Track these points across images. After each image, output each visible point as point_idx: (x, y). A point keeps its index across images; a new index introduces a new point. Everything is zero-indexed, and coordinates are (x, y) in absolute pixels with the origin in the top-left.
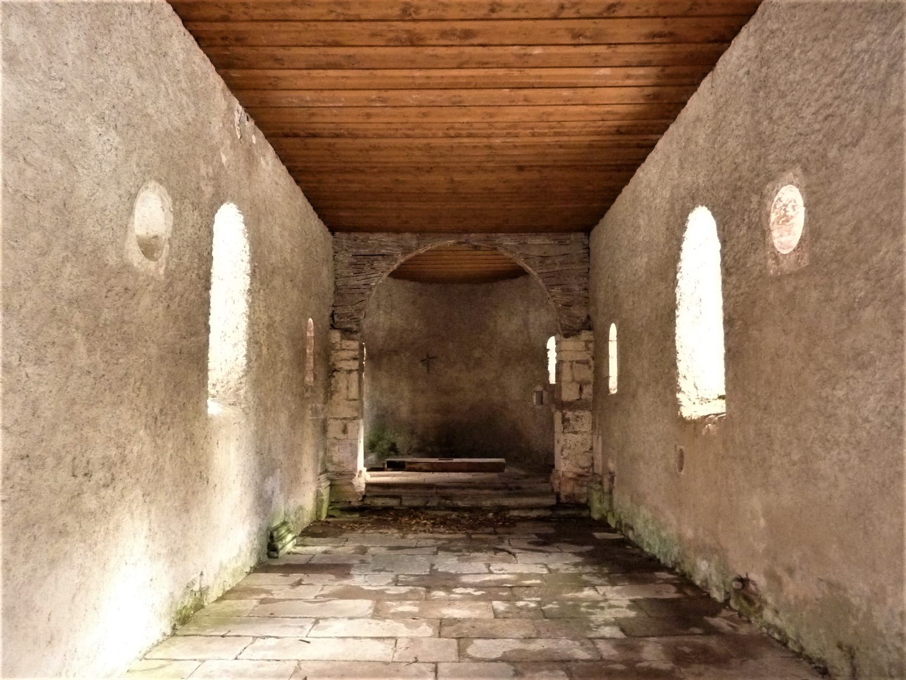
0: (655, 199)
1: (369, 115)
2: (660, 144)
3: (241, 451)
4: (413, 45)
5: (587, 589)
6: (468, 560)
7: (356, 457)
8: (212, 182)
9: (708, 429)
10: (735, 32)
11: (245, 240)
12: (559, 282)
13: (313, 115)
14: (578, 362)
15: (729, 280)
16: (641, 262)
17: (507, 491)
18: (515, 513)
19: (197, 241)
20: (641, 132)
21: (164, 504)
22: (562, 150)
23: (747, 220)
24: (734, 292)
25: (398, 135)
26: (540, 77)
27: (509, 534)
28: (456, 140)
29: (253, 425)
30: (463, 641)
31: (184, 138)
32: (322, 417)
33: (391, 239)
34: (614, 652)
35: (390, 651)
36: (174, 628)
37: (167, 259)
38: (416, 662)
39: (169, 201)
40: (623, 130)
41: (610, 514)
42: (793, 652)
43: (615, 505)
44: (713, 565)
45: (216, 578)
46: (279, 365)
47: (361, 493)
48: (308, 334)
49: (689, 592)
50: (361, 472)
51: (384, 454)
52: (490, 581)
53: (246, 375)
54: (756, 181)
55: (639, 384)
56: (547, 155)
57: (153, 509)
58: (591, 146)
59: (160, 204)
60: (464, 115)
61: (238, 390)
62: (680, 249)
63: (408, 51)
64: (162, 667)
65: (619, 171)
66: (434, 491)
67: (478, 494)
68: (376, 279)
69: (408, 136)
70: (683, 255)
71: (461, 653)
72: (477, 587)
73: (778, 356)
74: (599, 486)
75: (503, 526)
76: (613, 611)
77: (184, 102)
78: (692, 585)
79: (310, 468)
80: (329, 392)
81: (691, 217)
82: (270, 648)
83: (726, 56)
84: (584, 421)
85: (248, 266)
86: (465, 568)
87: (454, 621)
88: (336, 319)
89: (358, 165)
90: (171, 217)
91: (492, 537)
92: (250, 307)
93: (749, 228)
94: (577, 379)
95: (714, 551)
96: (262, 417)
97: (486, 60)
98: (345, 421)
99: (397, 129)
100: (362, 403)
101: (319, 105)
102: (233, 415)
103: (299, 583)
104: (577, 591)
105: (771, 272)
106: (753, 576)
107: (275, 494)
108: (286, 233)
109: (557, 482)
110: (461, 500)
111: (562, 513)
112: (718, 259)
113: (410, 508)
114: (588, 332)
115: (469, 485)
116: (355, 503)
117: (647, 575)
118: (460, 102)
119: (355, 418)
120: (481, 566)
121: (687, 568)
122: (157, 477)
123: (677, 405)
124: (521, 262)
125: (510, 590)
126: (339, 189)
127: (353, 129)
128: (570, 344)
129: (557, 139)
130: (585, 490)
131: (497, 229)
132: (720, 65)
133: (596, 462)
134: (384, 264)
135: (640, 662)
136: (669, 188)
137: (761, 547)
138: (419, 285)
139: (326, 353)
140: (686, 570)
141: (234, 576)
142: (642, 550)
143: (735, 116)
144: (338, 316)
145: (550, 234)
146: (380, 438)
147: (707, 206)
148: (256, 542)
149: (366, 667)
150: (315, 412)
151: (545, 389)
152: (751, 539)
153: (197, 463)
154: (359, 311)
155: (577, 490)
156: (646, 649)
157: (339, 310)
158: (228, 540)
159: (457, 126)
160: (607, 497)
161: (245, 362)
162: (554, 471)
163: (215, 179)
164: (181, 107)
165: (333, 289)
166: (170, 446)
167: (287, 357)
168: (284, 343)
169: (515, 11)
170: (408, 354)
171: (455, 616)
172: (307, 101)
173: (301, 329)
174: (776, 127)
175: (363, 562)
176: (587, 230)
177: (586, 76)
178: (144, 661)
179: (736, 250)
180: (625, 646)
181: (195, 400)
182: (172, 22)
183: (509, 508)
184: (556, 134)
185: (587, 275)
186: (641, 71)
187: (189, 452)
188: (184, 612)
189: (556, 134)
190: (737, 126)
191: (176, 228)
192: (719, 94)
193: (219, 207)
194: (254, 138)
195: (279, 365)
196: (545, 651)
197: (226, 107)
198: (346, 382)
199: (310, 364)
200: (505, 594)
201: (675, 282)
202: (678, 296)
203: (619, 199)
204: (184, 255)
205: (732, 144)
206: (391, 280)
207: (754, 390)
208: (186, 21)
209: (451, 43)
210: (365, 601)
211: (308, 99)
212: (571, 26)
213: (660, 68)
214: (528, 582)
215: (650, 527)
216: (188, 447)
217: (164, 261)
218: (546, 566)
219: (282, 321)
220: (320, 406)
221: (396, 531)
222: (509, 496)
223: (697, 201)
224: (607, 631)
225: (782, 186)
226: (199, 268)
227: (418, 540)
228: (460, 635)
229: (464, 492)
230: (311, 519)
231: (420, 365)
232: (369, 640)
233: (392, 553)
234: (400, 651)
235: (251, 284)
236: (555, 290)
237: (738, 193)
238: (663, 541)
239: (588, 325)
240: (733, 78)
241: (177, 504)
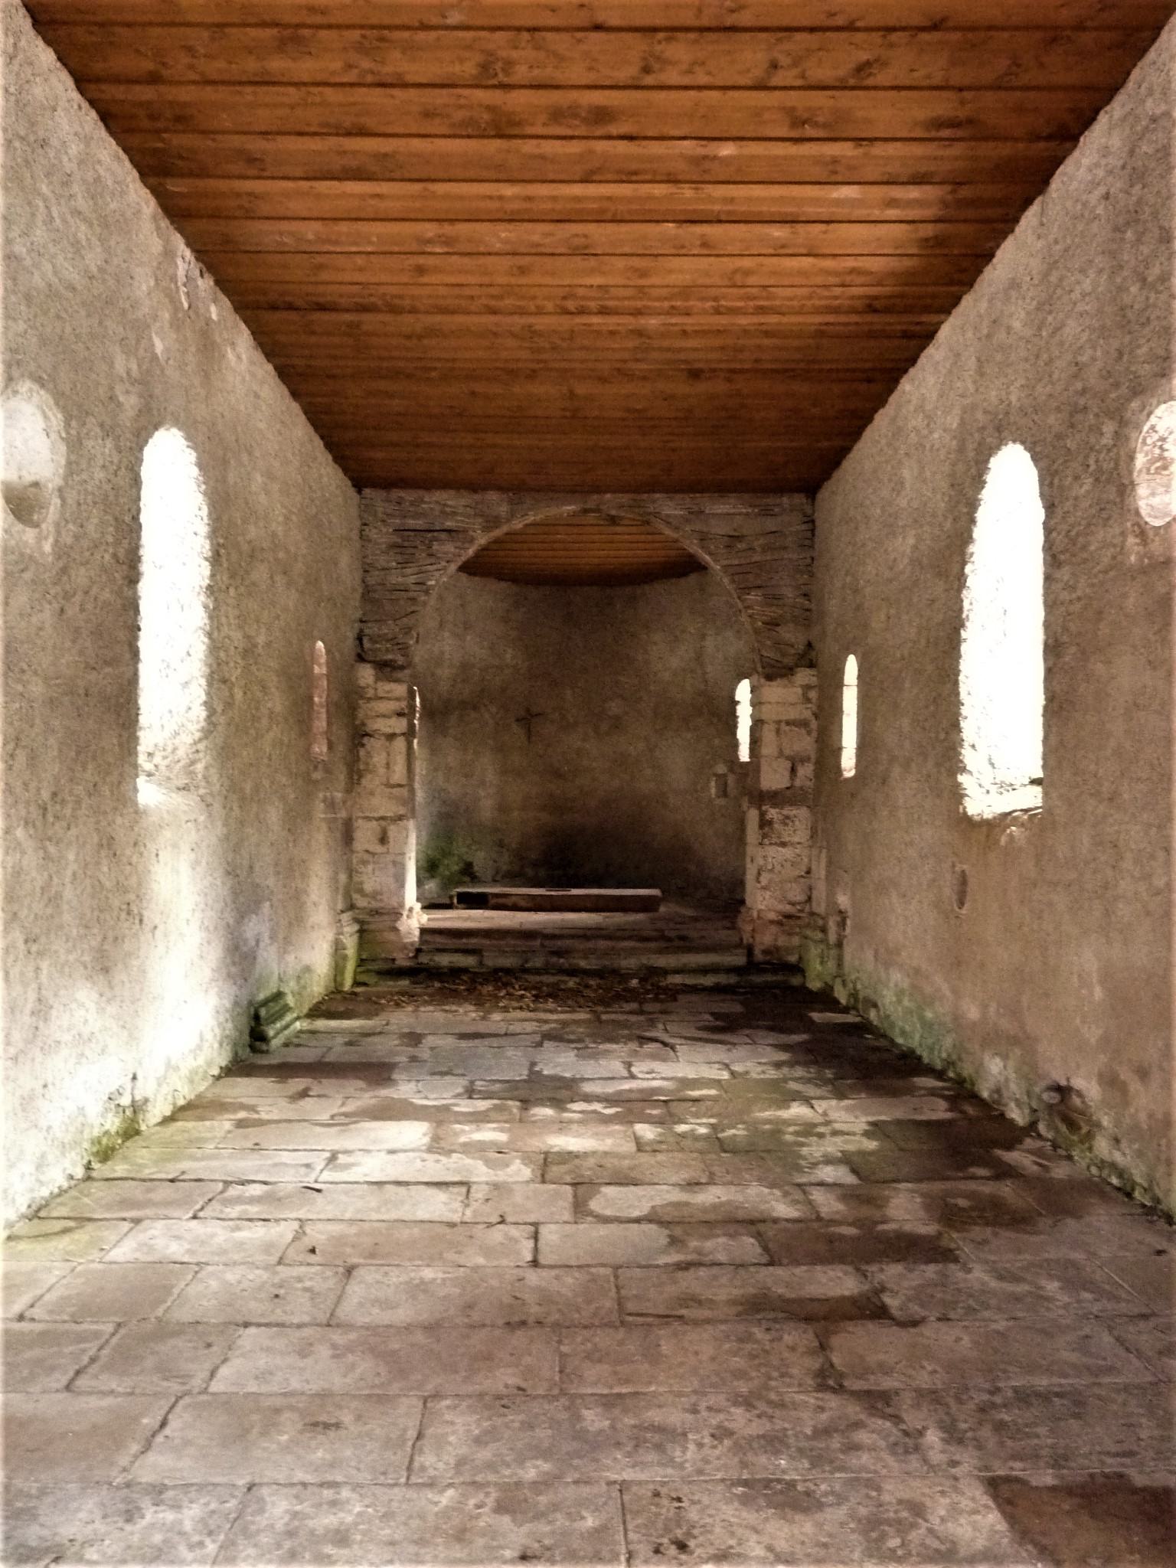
0: (931, 433)
1: (421, 270)
2: (945, 332)
3: (198, 869)
4: (501, 136)
5: (795, 1104)
6: (595, 1056)
7: (401, 884)
8: (137, 388)
9: (1011, 835)
10: (1087, 120)
11: (200, 498)
12: (759, 582)
13: (321, 267)
14: (788, 723)
15: (1057, 575)
16: (904, 545)
17: (663, 944)
18: (677, 979)
19: (111, 494)
20: (908, 310)
21: (63, 957)
22: (766, 342)
23: (1093, 467)
24: (1065, 596)
25: (473, 308)
26: (732, 200)
27: (664, 1012)
28: (579, 320)
29: (219, 824)
30: (582, 1189)
31: (84, 304)
32: (343, 814)
33: (463, 502)
34: (840, 1207)
35: (457, 1205)
36: (88, 1167)
37: (57, 525)
38: (502, 1222)
39: (57, 419)
40: (877, 304)
41: (838, 982)
42: (1144, 1206)
43: (846, 969)
44: (1011, 1063)
45: (159, 1085)
46: (265, 721)
47: (412, 944)
48: (317, 670)
49: (970, 1110)
50: (411, 910)
51: (451, 878)
52: (630, 1091)
53: (206, 738)
54: (1113, 395)
55: (893, 759)
56: (741, 350)
57: (45, 965)
58: (820, 334)
59: (41, 424)
60: (592, 271)
61: (193, 763)
62: (973, 521)
63: (492, 146)
64: (65, 1231)
65: (869, 381)
66: (538, 942)
67: (613, 948)
68: (437, 574)
69: (494, 312)
70: (977, 532)
71: (580, 1208)
72: (608, 1100)
73: (1136, 705)
74: (820, 935)
75: (656, 999)
76: (838, 1139)
77: (81, 236)
78: (974, 1097)
79: (323, 901)
80: (355, 773)
81: (994, 463)
82: (252, 1200)
83: (1067, 168)
84: (798, 824)
85: (207, 545)
86: (588, 1068)
87: (567, 1157)
88: (367, 644)
89: (401, 364)
90: (63, 448)
91: (633, 1018)
92: (211, 618)
93: (1097, 480)
94: (787, 752)
95: (1015, 1041)
96: (237, 811)
97: (634, 166)
98: (383, 823)
99: (472, 297)
100: (412, 791)
101: (332, 249)
102: (186, 808)
103: (304, 1094)
104: (780, 1108)
105: (1133, 558)
106: (1078, 1083)
107: (262, 945)
108: (276, 487)
109: (748, 928)
110: (586, 958)
111: (758, 979)
112: (1039, 538)
113: (496, 970)
114: (808, 671)
115: (586, 934)
116: (402, 961)
117: (899, 1083)
118: (586, 247)
119: (400, 818)
120: (616, 1066)
121: (967, 1070)
122: (49, 911)
123: (957, 795)
124: (694, 548)
125: (664, 1107)
126: (372, 407)
127: (394, 296)
128: (775, 691)
129: (763, 319)
130: (796, 941)
131: (652, 487)
132: (1056, 183)
133: (815, 894)
134: (450, 548)
135: (883, 1222)
136: (957, 411)
137: (1093, 1034)
138: (515, 588)
139: (348, 705)
140: (965, 1074)
141: (191, 1081)
142: (892, 1041)
143: (1079, 276)
144: (372, 640)
145: (746, 496)
146: (446, 853)
147: (1023, 443)
148: (230, 1025)
149: (416, 1231)
150: (331, 805)
151: (731, 770)
152: (1078, 1021)
153: (121, 888)
154: (407, 630)
155: (782, 941)
156: (894, 1202)
157: (372, 629)
158: (176, 1015)
159: (581, 292)
160: (833, 952)
161: (204, 714)
162: (743, 910)
163: (144, 382)
164: (76, 244)
165: (360, 590)
166: (71, 857)
167: (278, 708)
168: (272, 681)
169: (690, 72)
170: (494, 710)
171: (571, 1148)
172: (309, 241)
173: (305, 660)
174: (1153, 296)
175: (414, 1059)
176: (811, 488)
177: (816, 201)
178: (36, 1221)
179: (1071, 520)
180: (858, 1196)
181: (114, 778)
182: (54, 80)
183: (665, 972)
184: (761, 310)
185: (809, 568)
186: (914, 193)
187: (105, 869)
188: (104, 1141)
189: (761, 310)
190: (1084, 295)
191: (71, 468)
192: (1051, 237)
193: (150, 435)
194: (213, 309)
195: (265, 721)
196: (722, 1204)
197: (160, 248)
198: (384, 754)
199: (320, 723)
200: (655, 1112)
201: (961, 580)
202: (966, 605)
203: (869, 433)
204: (88, 519)
205: (1072, 328)
206: (464, 577)
207: (1092, 767)
208: (82, 81)
209: (570, 132)
210: (416, 1124)
211: (311, 236)
212: (789, 104)
213: (948, 188)
214: (696, 1093)
215: (906, 1002)
216: (105, 862)
217: (52, 529)
218: (727, 1066)
219: (268, 644)
220: (339, 795)
221: (472, 1008)
222: (660, 952)
223: (1005, 434)
224: (828, 1173)
225: (1159, 404)
226: (117, 543)
227: (509, 1022)
228: (580, 1183)
229: (590, 945)
230: (326, 987)
231: (515, 728)
232: (423, 1187)
233: (464, 1044)
234: (475, 1205)
235: (213, 576)
236: (753, 597)
237: (1079, 417)
238: (927, 1025)
239: (808, 658)
240: (1079, 207)
241: (87, 958)
